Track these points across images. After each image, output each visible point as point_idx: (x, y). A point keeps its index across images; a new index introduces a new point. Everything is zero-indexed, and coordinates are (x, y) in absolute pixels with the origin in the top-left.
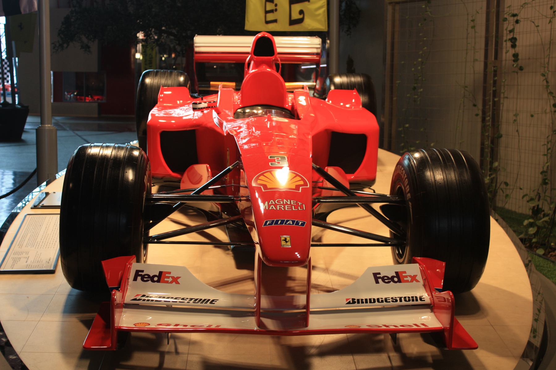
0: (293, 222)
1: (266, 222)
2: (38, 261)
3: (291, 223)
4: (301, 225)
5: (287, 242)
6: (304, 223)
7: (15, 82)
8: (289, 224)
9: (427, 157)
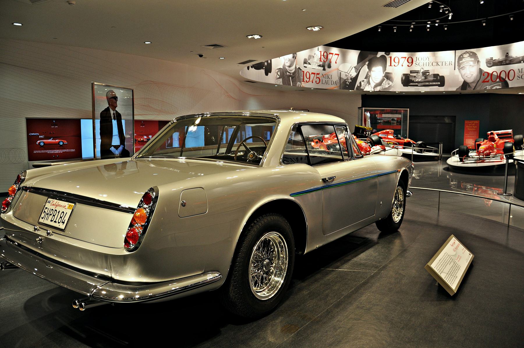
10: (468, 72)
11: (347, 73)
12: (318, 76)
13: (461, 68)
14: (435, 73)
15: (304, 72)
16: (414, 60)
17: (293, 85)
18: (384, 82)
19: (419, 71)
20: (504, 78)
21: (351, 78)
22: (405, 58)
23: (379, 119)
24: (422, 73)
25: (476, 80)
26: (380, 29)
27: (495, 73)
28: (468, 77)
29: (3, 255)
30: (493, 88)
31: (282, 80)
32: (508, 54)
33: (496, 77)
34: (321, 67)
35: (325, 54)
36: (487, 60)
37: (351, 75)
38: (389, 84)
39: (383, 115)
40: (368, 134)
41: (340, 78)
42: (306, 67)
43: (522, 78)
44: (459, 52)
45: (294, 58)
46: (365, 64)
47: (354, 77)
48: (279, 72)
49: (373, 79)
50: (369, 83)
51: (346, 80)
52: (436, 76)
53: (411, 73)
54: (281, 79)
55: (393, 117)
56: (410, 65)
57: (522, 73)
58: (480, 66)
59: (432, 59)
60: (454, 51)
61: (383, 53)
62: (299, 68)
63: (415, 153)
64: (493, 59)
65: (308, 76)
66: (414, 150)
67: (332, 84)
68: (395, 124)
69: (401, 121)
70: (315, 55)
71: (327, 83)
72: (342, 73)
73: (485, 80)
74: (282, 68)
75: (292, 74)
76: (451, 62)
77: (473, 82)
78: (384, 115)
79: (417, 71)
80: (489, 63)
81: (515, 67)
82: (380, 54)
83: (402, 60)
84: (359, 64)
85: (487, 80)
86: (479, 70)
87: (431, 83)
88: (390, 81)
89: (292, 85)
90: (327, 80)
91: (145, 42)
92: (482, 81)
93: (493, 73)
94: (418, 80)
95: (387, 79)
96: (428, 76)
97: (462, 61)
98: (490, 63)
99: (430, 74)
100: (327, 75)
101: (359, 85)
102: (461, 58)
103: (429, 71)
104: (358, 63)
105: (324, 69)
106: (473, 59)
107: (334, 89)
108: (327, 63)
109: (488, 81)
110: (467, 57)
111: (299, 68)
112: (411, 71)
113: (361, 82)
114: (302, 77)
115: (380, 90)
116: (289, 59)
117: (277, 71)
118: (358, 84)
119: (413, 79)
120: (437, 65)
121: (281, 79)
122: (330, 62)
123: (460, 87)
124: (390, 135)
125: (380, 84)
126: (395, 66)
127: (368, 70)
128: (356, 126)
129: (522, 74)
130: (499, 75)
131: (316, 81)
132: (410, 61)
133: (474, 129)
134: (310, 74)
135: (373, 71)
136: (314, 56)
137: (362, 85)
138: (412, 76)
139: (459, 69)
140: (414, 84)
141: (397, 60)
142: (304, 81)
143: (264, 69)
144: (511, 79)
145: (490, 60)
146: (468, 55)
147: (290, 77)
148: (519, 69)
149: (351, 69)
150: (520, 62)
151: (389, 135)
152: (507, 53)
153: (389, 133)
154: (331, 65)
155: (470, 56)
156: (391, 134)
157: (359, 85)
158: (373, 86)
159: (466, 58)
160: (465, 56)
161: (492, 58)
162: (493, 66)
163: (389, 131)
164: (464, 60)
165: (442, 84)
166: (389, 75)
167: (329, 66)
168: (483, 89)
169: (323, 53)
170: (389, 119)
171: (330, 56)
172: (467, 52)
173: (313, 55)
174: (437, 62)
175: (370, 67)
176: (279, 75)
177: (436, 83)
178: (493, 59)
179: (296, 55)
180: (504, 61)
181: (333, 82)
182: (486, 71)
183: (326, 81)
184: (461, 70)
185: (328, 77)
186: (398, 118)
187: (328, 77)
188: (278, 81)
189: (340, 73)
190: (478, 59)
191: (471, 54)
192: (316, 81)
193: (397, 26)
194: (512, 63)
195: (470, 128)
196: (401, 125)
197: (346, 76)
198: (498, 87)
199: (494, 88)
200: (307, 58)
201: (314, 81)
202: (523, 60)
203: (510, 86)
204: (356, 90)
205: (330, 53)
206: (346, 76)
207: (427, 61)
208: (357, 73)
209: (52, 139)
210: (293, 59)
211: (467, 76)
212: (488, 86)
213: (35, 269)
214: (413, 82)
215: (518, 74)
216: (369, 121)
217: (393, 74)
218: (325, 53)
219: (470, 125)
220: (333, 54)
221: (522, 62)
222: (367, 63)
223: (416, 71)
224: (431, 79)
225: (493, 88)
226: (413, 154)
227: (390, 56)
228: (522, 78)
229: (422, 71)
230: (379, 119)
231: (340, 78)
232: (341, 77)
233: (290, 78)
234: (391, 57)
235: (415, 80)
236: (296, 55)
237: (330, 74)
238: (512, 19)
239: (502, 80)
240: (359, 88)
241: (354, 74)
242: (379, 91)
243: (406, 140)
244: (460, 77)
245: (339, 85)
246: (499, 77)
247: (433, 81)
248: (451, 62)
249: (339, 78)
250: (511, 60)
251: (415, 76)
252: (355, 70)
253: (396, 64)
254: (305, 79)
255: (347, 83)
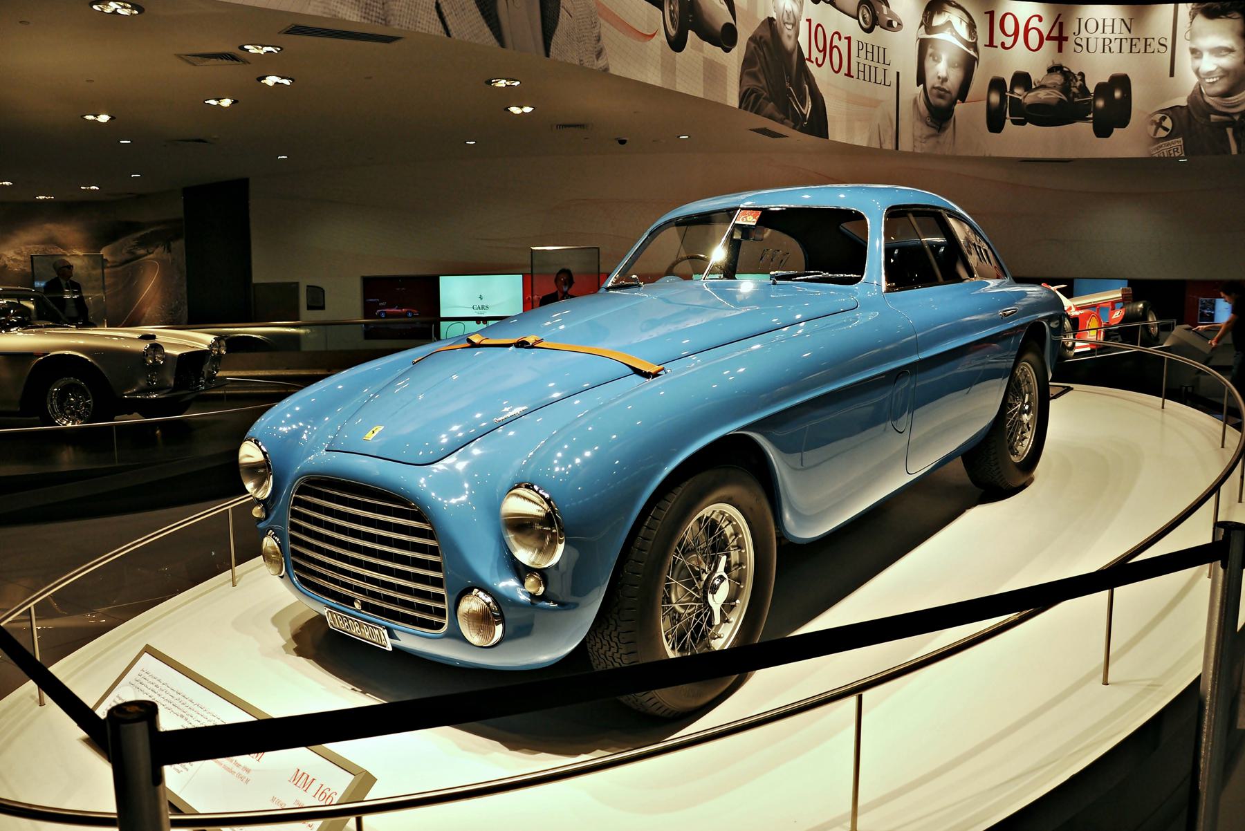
29: (505, 403)
43: (1088, 50)
54: (1181, 139)
60: (1173, 5)
91: (679, 137)
117: (1159, 116)
121: (1181, 139)
143: (1090, 119)
147: (1229, 126)
188: (1161, 146)
209: (397, 309)
213: (579, 401)
233: (1229, 131)
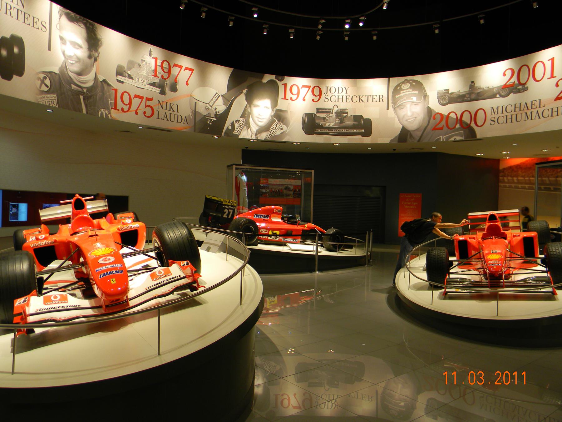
0: (116, 271)
1: (101, 275)
2: (278, 145)
3: (115, 273)
4: (121, 273)
5: (114, 281)
6: (122, 271)
7: (545, 266)
8: (114, 273)
9: (529, 186)
10: (409, 114)
11: (208, 105)
12: (149, 103)
13: (397, 107)
14: (356, 114)
15: (116, 90)
16: (324, 91)
17: (87, 113)
18: (274, 126)
19: (332, 110)
20: (469, 123)
21: (216, 115)
22: (309, 87)
23: (264, 188)
24: (335, 113)
25: (421, 126)
26: (265, 30)
27: (453, 115)
28: (408, 121)
30: (450, 140)
31: (56, 98)
32: (473, 84)
33: (455, 121)
34: (157, 87)
35: (166, 65)
36: (439, 93)
37: (216, 109)
38: (282, 129)
39: (270, 180)
40: (227, 213)
41: (195, 112)
42: (122, 82)
43: (498, 122)
44: (395, 81)
45: (93, 59)
46: (242, 93)
47: (220, 112)
48: (48, 79)
49: (256, 119)
50: (248, 126)
51: (207, 117)
52: (358, 118)
53: (317, 112)
55: (286, 184)
56: (316, 99)
57: (498, 114)
58: (428, 103)
59: (350, 92)
60: (387, 79)
61: (273, 77)
62: (104, 81)
63: (324, 253)
64: (450, 93)
65: (126, 100)
66: (322, 246)
67: (180, 120)
68: (291, 197)
69: (300, 190)
70: (144, 63)
71: (169, 119)
72: (199, 104)
73: (437, 127)
74: (58, 72)
75: (85, 91)
76: (381, 97)
77: (417, 130)
78: (271, 181)
79: (328, 110)
80: (442, 99)
81: (486, 104)
82: (267, 78)
83: (303, 91)
84: (228, 92)
85: (440, 126)
86: (426, 110)
87: (350, 131)
88: (284, 124)
89: (84, 112)
90: (168, 112)
92: (432, 128)
93: (451, 115)
94: (329, 125)
95: (278, 121)
96: (345, 119)
97: (399, 96)
98: (445, 99)
99: (349, 115)
100: (168, 105)
101: (230, 128)
102: (397, 90)
103: (347, 111)
104: (229, 89)
105: (163, 93)
106: (417, 92)
107: (183, 130)
108: (169, 82)
109: (441, 129)
110: (406, 88)
111: (104, 81)
112: (318, 109)
113: (235, 122)
114: (111, 100)
115: (267, 138)
116: (78, 58)
117: (42, 76)
118: (228, 124)
119: (321, 123)
120: (359, 102)
121: (55, 95)
122: (176, 81)
123: (395, 137)
124: (276, 215)
125: (267, 128)
126: (293, 99)
127: (246, 103)
128: (208, 197)
129: (498, 116)
130: (459, 118)
131: (145, 113)
132: (317, 92)
133: (413, 207)
134: (132, 98)
135: (254, 106)
136: (141, 65)
137: (235, 129)
138: (320, 118)
139: (394, 108)
140: (323, 131)
141: (295, 90)
142: (115, 108)
144: (479, 123)
145: (444, 93)
146: (409, 85)
147: (82, 95)
148: (493, 108)
149: (215, 99)
150: (494, 96)
151: (274, 217)
152: (473, 82)
153: (273, 213)
154: (177, 86)
155: (412, 87)
156: (276, 213)
157: (230, 128)
158: (255, 131)
159: (405, 91)
160: (404, 87)
161: (449, 90)
162: (449, 103)
163: (273, 209)
164: (402, 94)
165: (368, 132)
166: (281, 113)
167: (174, 89)
168: (434, 141)
169: (161, 62)
170: (280, 188)
171: (175, 71)
172: (408, 81)
173: (140, 62)
174: (360, 96)
175: (250, 99)
176: (49, 85)
177: (359, 131)
178: (450, 93)
179: (96, 54)
180: (467, 96)
181: (180, 118)
182: (437, 111)
183: (166, 113)
184: (398, 109)
185: (171, 107)
186: (296, 186)
187: (171, 107)
188: (44, 97)
189: (196, 103)
190: (425, 91)
191: (414, 84)
192: (145, 113)
193: (296, 29)
194: (480, 98)
195: (408, 205)
196: (301, 197)
197: (207, 109)
198: (458, 138)
199: (452, 139)
200: (125, 65)
201: (140, 112)
202: (499, 93)
203: (478, 136)
204: (224, 135)
205: (175, 65)
206: (206, 109)
207: (344, 94)
208: (226, 106)
210: (88, 60)
211: (407, 120)
212: (441, 137)
214: (321, 127)
215: (492, 116)
216: (244, 191)
217: (289, 112)
218: (164, 62)
219: (407, 200)
220: (181, 67)
221: (498, 96)
222: (245, 91)
223: (327, 109)
224: (350, 123)
225: (449, 139)
226: (319, 254)
227: (284, 82)
228: (498, 122)
229: (336, 109)
230: (264, 188)
231: (195, 112)
232: (197, 110)
234: (285, 85)
235: (325, 124)
236: (96, 54)
237: (176, 103)
238: (482, 22)
239: (465, 126)
240: (230, 132)
241: (221, 107)
242: (265, 141)
243: (306, 226)
244: (396, 119)
245: (193, 124)
246: (460, 121)
247: (354, 127)
248: (381, 97)
249: (192, 112)
250: (478, 93)
251: (324, 118)
252: (224, 102)
253: (294, 97)
254: (120, 105)
255: (208, 122)
